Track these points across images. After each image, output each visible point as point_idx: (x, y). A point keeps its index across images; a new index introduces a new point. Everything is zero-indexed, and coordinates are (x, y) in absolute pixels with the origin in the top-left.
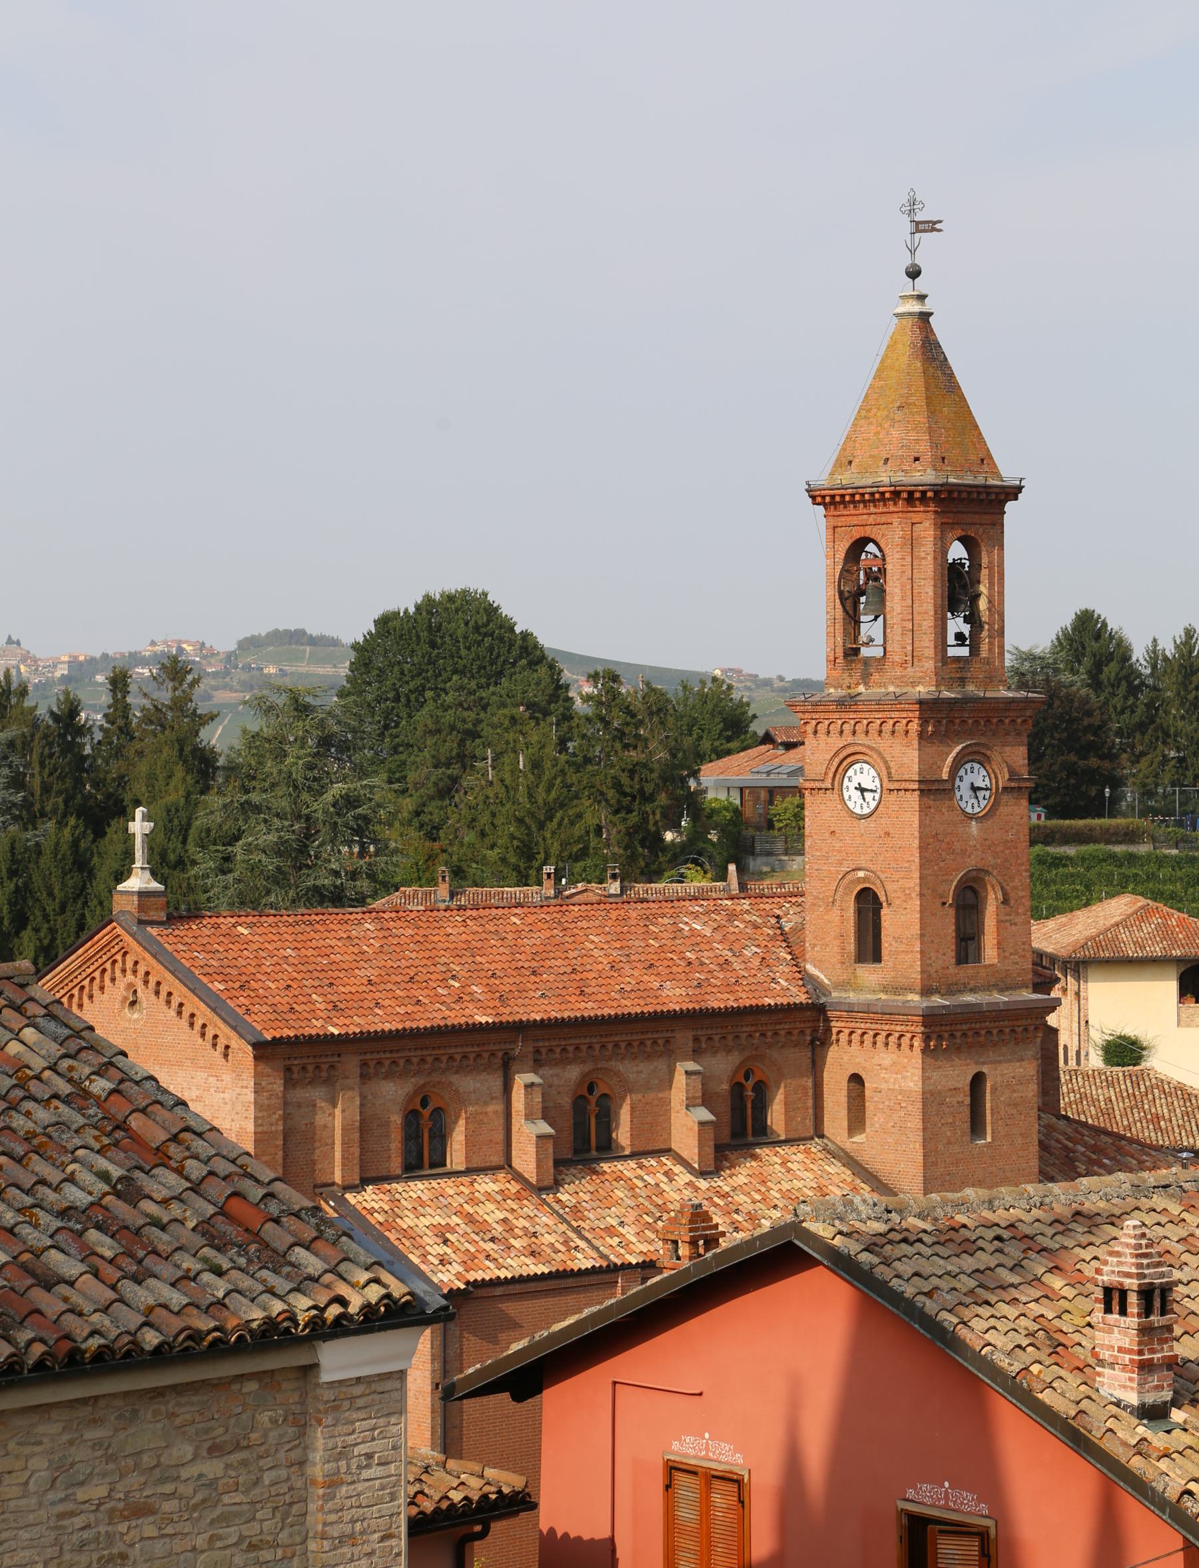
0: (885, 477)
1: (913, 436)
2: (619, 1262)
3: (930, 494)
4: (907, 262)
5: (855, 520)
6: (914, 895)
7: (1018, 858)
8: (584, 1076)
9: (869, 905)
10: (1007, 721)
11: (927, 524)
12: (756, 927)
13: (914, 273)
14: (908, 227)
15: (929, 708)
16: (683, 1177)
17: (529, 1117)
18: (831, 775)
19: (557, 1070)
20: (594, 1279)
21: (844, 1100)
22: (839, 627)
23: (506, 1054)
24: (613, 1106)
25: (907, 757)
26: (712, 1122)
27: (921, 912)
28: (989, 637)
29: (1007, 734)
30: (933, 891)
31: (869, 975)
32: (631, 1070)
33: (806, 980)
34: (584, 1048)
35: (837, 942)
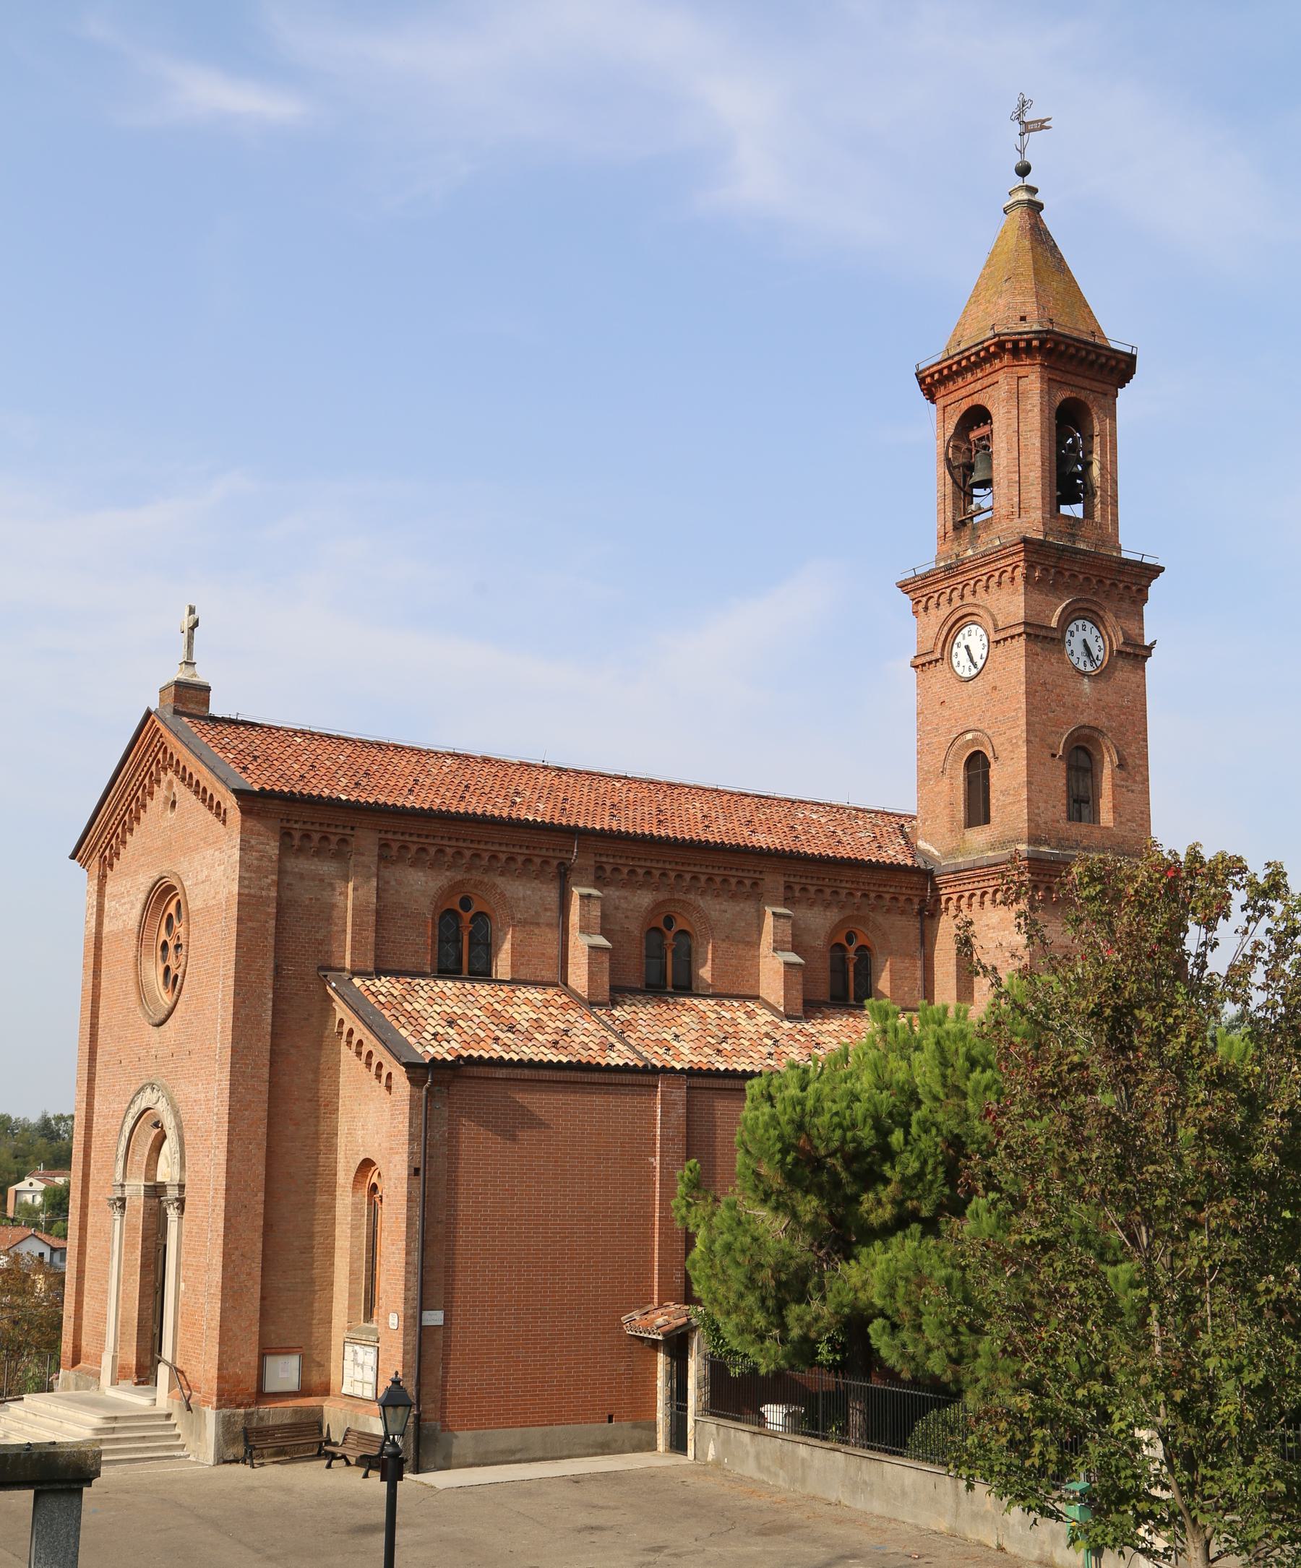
1: (1020, 299)
2: (659, 1065)
3: (1035, 343)
4: (1016, 160)
5: (964, 392)
6: (1020, 743)
7: (1135, 726)
8: (658, 905)
9: (977, 765)
10: (1121, 586)
11: (1033, 377)
13: (1024, 170)
14: (1017, 128)
17: (585, 929)
18: (940, 645)
19: (623, 893)
20: (627, 1078)
21: (953, 969)
22: (949, 502)
23: (562, 864)
24: (693, 945)
25: (1011, 603)
26: (800, 965)
27: (1028, 758)
28: (1102, 503)
29: (1121, 599)
30: (1042, 740)
31: (979, 837)
32: (717, 909)
34: (657, 873)
35: (947, 811)
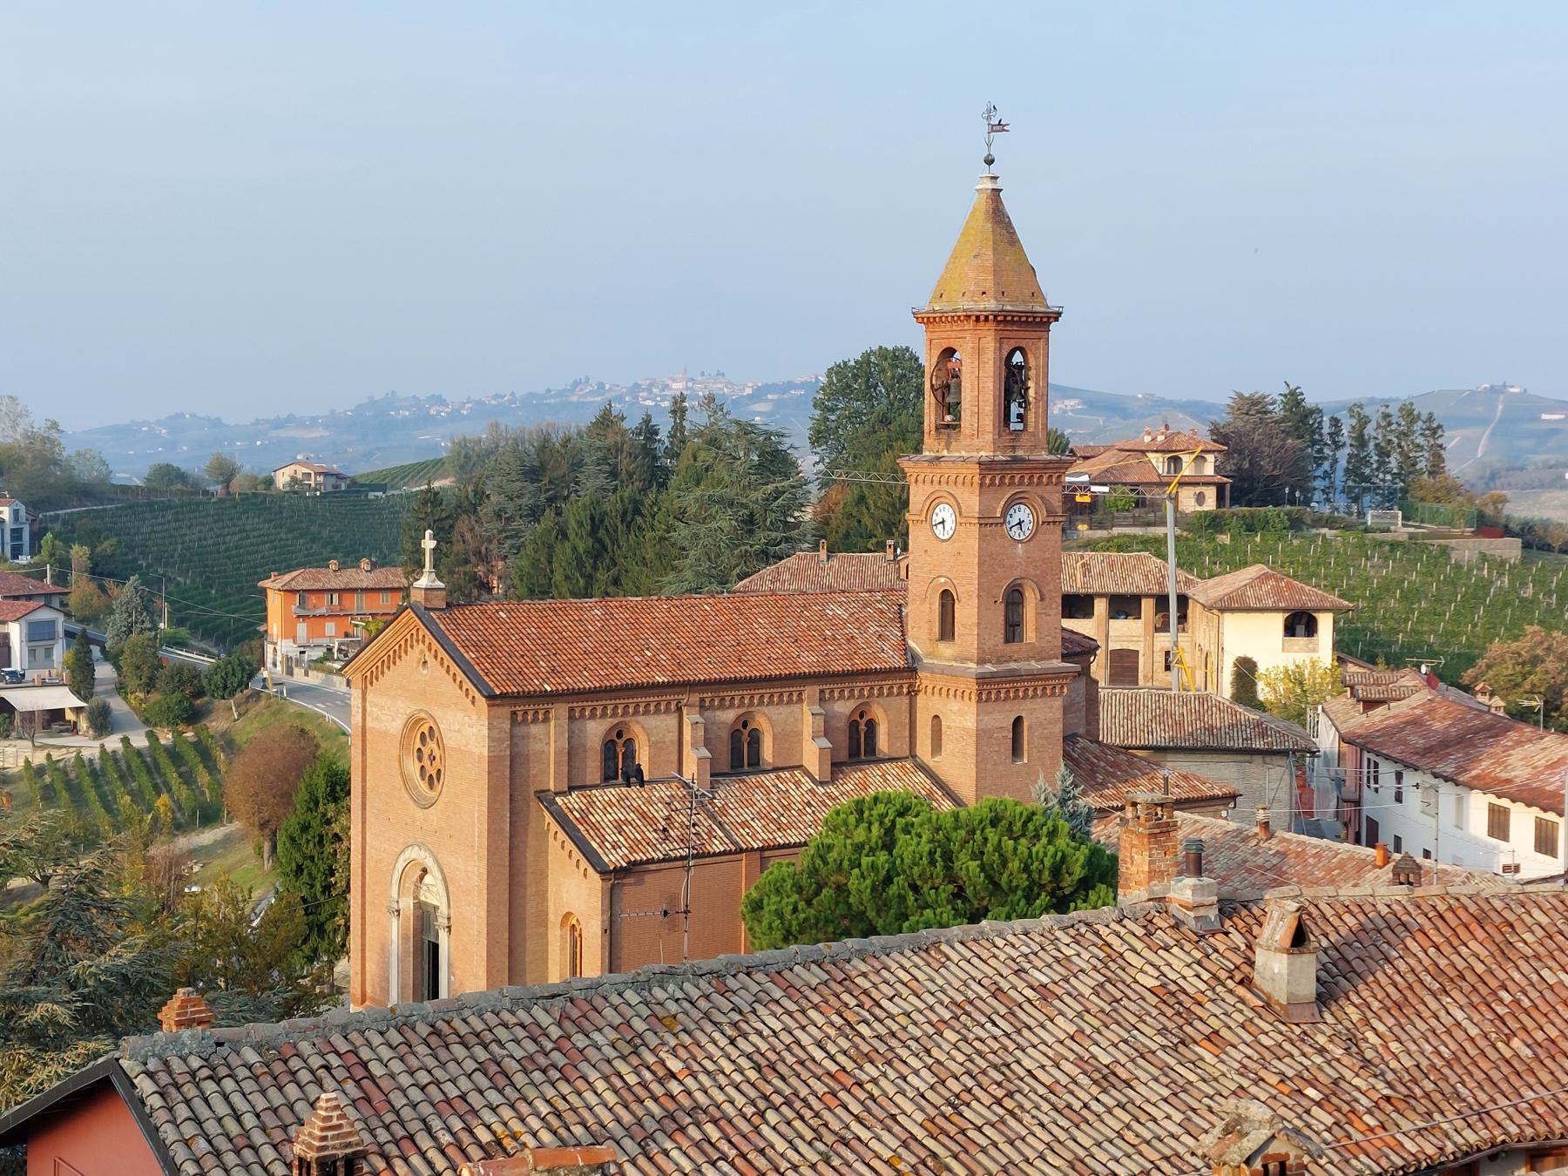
0: (965, 304)
5: (944, 335)
12: (882, 612)
13: (989, 161)
14: (987, 129)
15: (986, 466)
16: (807, 784)
25: (972, 501)
31: (946, 649)
33: (906, 649)
